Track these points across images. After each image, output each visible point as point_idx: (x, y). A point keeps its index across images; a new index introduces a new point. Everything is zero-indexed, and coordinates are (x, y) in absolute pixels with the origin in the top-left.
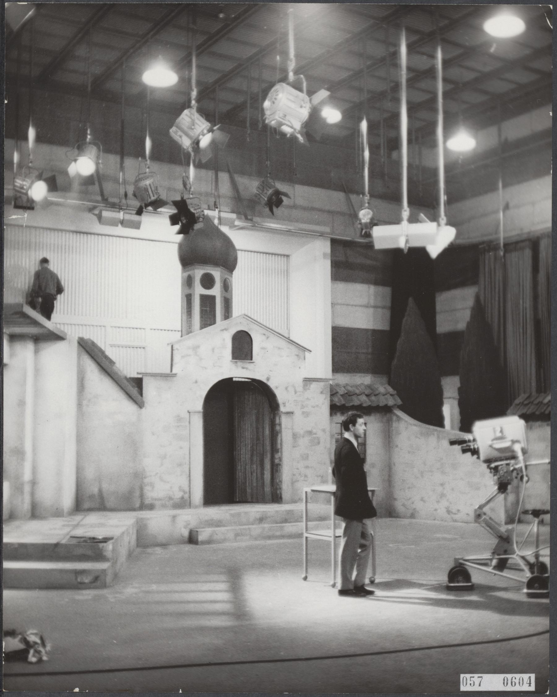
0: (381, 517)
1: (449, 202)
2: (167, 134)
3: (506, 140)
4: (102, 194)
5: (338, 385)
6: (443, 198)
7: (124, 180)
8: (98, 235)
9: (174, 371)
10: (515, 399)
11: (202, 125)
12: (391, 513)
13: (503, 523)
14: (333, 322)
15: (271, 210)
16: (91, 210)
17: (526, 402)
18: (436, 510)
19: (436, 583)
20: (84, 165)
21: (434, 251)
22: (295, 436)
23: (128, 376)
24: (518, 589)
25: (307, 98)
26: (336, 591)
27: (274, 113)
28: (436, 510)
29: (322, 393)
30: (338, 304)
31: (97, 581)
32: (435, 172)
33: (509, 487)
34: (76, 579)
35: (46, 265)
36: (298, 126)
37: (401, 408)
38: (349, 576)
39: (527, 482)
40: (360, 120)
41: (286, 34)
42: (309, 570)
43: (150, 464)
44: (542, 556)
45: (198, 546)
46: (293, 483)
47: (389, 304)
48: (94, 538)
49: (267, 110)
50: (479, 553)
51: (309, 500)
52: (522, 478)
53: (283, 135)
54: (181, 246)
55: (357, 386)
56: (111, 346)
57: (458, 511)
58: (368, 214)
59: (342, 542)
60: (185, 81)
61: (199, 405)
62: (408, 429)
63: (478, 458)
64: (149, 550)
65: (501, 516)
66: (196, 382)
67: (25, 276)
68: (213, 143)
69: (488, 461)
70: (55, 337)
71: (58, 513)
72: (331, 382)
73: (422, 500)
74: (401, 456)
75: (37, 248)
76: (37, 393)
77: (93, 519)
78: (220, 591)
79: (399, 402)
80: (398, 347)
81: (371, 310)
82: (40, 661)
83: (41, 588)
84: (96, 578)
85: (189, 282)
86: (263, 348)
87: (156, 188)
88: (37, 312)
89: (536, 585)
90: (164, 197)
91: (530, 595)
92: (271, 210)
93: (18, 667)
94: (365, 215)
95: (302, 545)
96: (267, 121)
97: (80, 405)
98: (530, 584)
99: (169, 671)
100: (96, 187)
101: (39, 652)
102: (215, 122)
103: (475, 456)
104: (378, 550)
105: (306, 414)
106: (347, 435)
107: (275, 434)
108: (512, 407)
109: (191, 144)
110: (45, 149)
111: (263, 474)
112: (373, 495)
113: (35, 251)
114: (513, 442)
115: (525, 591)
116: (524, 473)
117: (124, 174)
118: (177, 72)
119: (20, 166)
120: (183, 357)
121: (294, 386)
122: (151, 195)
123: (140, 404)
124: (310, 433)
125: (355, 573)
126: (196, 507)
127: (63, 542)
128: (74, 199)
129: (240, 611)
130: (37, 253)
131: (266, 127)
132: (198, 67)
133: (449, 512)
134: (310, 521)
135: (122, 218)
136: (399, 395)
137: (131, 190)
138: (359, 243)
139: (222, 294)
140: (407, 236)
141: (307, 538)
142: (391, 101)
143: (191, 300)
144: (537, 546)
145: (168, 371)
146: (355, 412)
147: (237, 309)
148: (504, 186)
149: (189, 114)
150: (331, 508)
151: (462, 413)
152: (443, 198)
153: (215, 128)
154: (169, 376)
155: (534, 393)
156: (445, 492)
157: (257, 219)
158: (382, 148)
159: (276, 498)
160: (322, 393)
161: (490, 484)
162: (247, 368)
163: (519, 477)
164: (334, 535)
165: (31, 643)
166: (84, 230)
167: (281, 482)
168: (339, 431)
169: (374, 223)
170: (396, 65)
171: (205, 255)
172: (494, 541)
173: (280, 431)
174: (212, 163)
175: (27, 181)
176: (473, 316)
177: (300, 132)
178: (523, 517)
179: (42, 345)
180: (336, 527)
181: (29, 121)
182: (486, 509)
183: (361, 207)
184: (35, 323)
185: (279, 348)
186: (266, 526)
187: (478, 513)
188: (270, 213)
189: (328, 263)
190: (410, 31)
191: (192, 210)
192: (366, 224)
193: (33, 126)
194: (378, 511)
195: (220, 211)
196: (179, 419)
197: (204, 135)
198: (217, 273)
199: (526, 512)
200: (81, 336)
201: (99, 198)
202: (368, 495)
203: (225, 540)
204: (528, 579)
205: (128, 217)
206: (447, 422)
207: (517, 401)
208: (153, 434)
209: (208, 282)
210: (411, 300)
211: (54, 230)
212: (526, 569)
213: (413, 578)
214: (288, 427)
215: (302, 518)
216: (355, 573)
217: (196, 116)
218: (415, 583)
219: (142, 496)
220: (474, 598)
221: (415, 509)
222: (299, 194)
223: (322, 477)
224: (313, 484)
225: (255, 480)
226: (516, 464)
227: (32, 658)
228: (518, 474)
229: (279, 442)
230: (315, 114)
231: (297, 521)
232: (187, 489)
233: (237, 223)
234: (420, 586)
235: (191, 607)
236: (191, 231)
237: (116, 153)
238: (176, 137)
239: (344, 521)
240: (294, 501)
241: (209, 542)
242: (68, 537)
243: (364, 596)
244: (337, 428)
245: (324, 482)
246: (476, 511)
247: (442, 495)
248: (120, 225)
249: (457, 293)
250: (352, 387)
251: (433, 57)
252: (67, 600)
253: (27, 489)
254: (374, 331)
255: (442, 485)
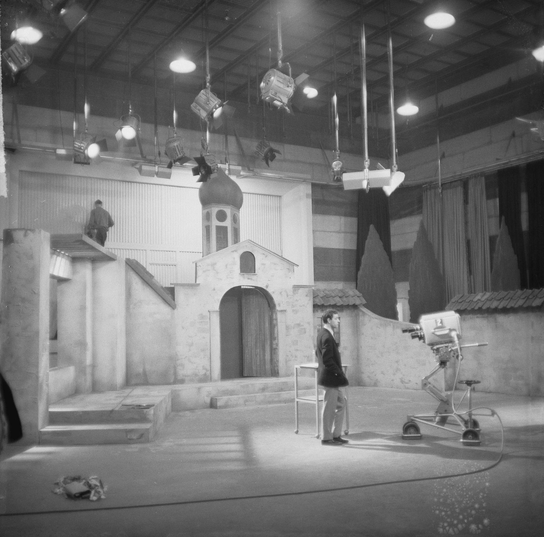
0: (352, 386)
1: (399, 154)
2: (189, 109)
3: (442, 106)
4: (142, 153)
5: (318, 290)
6: (395, 151)
7: (158, 142)
8: (139, 183)
9: (197, 283)
10: (451, 298)
11: (215, 101)
12: (360, 383)
13: (444, 390)
14: (314, 244)
15: (267, 163)
16: (133, 165)
17: (460, 301)
18: (393, 380)
19: (394, 434)
20: (128, 132)
21: (389, 190)
22: (287, 328)
23: (164, 286)
24: (456, 439)
25: (292, 80)
26: (320, 441)
27: (268, 92)
28: (393, 380)
29: (307, 296)
30: (317, 231)
31: (143, 437)
32: (388, 132)
33: (448, 363)
34: (127, 436)
35: (100, 205)
36: (285, 100)
37: (366, 306)
38: (329, 429)
39: (462, 360)
40: (333, 95)
41: (276, 32)
42: (300, 426)
43: (181, 350)
44: (474, 415)
45: (217, 410)
46: (286, 362)
47: (355, 230)
48: (140, 406)
49: (263, 89)
50: (425, 412)
51: (299, 374)
52: (457, 357)
53: (275, 107)
54: (201, 190)
55: (333, 291)
56: (151, 264)
57: (410, 381)
58: (339, 165)
59: (324, 405)
60: (200, 68)
61: (217, 306)
62: (371, 321)
63: (424, 342)
64: (181, 414)
65: (442, 385)
66: (214, 290)
67: (84, 213)
68: (223, 114)
69: (432, 344)
70: (109, 258)
71: (112, 388)
72: (313, 288)
73: (382, 373)
74: (366, 341)
75: (93, 193)
76: (95, 300)
77: (139, 391)
78: (234, 443)
79: (364, 302)
80: (362, 261)
81: (343, 235)
82: (99, 499)
83: (100, 444)
84: (142, 436)
85: (207, 217)
86: (263, 264)
87: (182, 148)
88: (94, 240)
89: (470, 436)
90: (188, 154)
91: (465, 444)
92: (267, 163)
93: (81, 504)
94: (336, 165)
95: (294, 408)
96: (262, 98)
97: (128, 308)
98: (466, 435)
99: (195, 505)
100: (137, 148)
101: (99, 492)
102: (224, 98)
103: (422, 341)
104: (350, 410)
105: (295, 312)
106: (326, 326)
107: (273, 326)
108: (449, 304)
109: (207, 116)
110: (98, 120)
111: (264, 356)
112: (346, 369)
113: (91, 195)
114: (451, 330)
115: (461, 440)
116: (460, 353)
117: (157, 138)
118: (195, 62)
119: (78, 131)
120: (204, 272)
121: (286, 291)
122: (178, 153)
123: (173, 306)
124: (299, 325)
125: (333, 428)
126: (216, 381)
127: (117, 409)
128: (120, 157)
129: (248, 457)
130: (93, 196)
131: (262, 102)
132: (211, 57)
133: (402, 382)
134: (300, 389)
135: (157, 171)
136: (364, 296)
137: (163, 150)
138: (333, 186)
139: (232, 225)
140: (368, 180)
141: (297, 402)
142: (354, 80)
143: (209, 229)
144: (470, 408)
145: (193, 282)
146: (331, 309)
147: (243, 236)
148: (441, 141)
149: (204, 93)
150: (315, 380)
151: (411, 309)
152: (395, 151)
153: (224, 103)
154: (194, 286)
155: (466, 293)
156: (399, 367)
157: (256, 170)
158: (349, 115)
159: (275, 373)
160: (307, 296)
161: (433, 362)
162: (251, 279)
163: (455, 356)
164: (318, 399)
165: (93, 486)
166: (128, 180)
167: (278, 361)
168: (320, 323)
169: (343, 171)
170: (358, 53)
171: (218, 196)
172: (437, 404)
173: (277, 324)
174: (222, 129)
175: (84, 144)
176: (419, 238)
177: (287, 105)
178: (459, 386)
179: (98, 264)
180: (319, 393)
181: (85, 99)
182: (430, 380)
183: (334, 160)
184: (93, 248)
185: (275, 264)
186: (267, 394)
187: (424, 382)
188: (266, 165)
189: (310, 201)
190: (369, 27)
191: (209, 164)
192: (337, 171)
193: (87, 103)
194: (349, 382)
195: (229, 165)
196: (202, 317)
197: (216, 109)
198: (228, 210)
199: (461, 382)
200: (128, 257)
201: (140, 156)
202: (341, 370)
203: (237, 405)
204: (463, 432)
205: (161, 170)
206: (400, 316)
207: (453, 300)
208: (183, 328)
209: (222, 216)
210: (372, 227)
211: (106, 179)
212: (462, 424)
213: (378, 431)
214: (281, 321)
215: (294, 387)
216: (333, 428)
217: (210, 94)
218: (378, 434)
219: (175, 374)
220: (422, 445)
221: (377, 380)
222: (287, 151)
223: (308, 357)
224: (302, 363)
225: (258, 361)
226: (453, 347)
227: (93, 497)
228: (454, 354)
229: (276, 332)
230: (298, 91)
231: (290, 390)
232: (208, 368)
233: (242, 173)
234: (382, 436)
235: (212, 456)
236: (208, 179)
237: (150, 122)
238: (196, 111)
239: (325, 389)
240: (288, 375)
241: (226, 406)
242: (121, 405)
243: (341, 445)
244: (319, 321)
245: (310, 361)
246: (422, 381)
247: (398, 370)
248: (155, 176)
249: (406, 221)
250: (329, 291)
251: (386, 46)
252: (120, 452)
253: (89, 371)
254: (344, 250)
255: (397, 362)
